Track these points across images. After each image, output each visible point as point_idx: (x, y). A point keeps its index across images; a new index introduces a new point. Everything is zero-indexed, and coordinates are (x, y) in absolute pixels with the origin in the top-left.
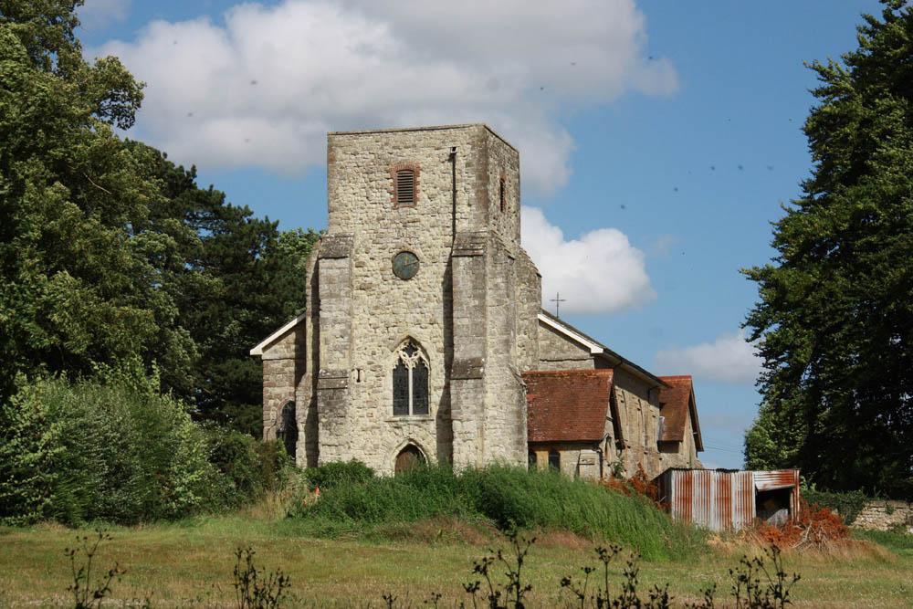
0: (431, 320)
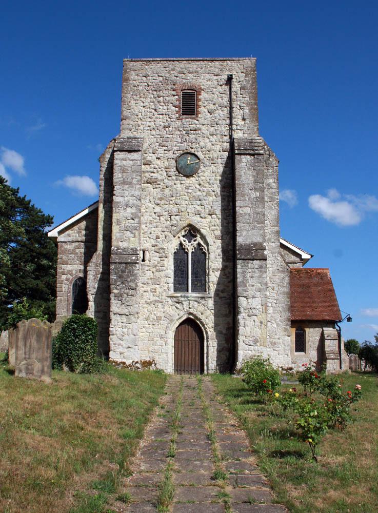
0: (210, 211)
